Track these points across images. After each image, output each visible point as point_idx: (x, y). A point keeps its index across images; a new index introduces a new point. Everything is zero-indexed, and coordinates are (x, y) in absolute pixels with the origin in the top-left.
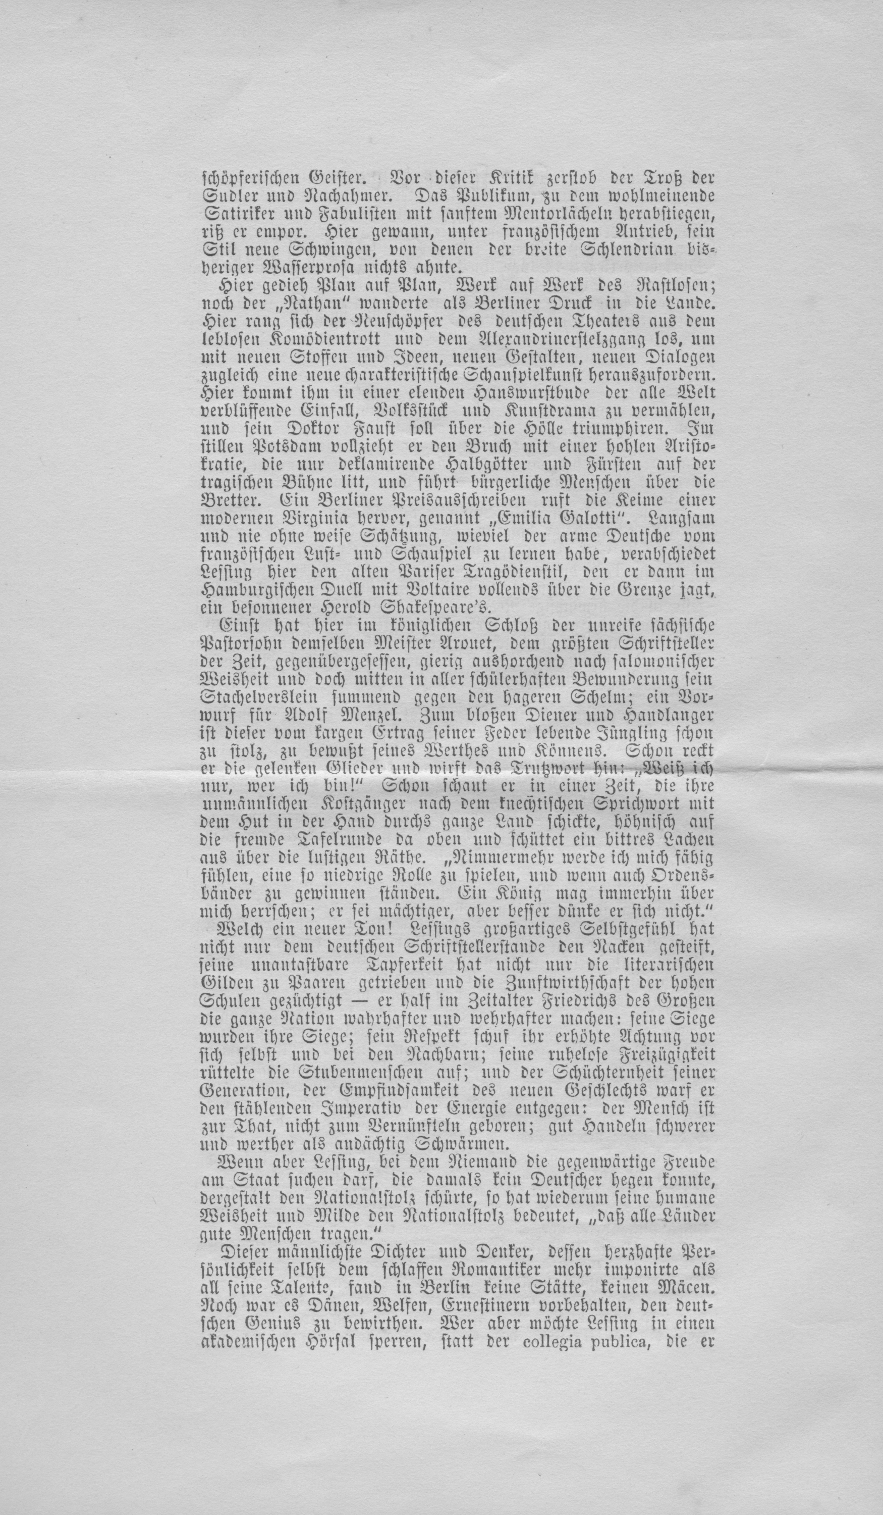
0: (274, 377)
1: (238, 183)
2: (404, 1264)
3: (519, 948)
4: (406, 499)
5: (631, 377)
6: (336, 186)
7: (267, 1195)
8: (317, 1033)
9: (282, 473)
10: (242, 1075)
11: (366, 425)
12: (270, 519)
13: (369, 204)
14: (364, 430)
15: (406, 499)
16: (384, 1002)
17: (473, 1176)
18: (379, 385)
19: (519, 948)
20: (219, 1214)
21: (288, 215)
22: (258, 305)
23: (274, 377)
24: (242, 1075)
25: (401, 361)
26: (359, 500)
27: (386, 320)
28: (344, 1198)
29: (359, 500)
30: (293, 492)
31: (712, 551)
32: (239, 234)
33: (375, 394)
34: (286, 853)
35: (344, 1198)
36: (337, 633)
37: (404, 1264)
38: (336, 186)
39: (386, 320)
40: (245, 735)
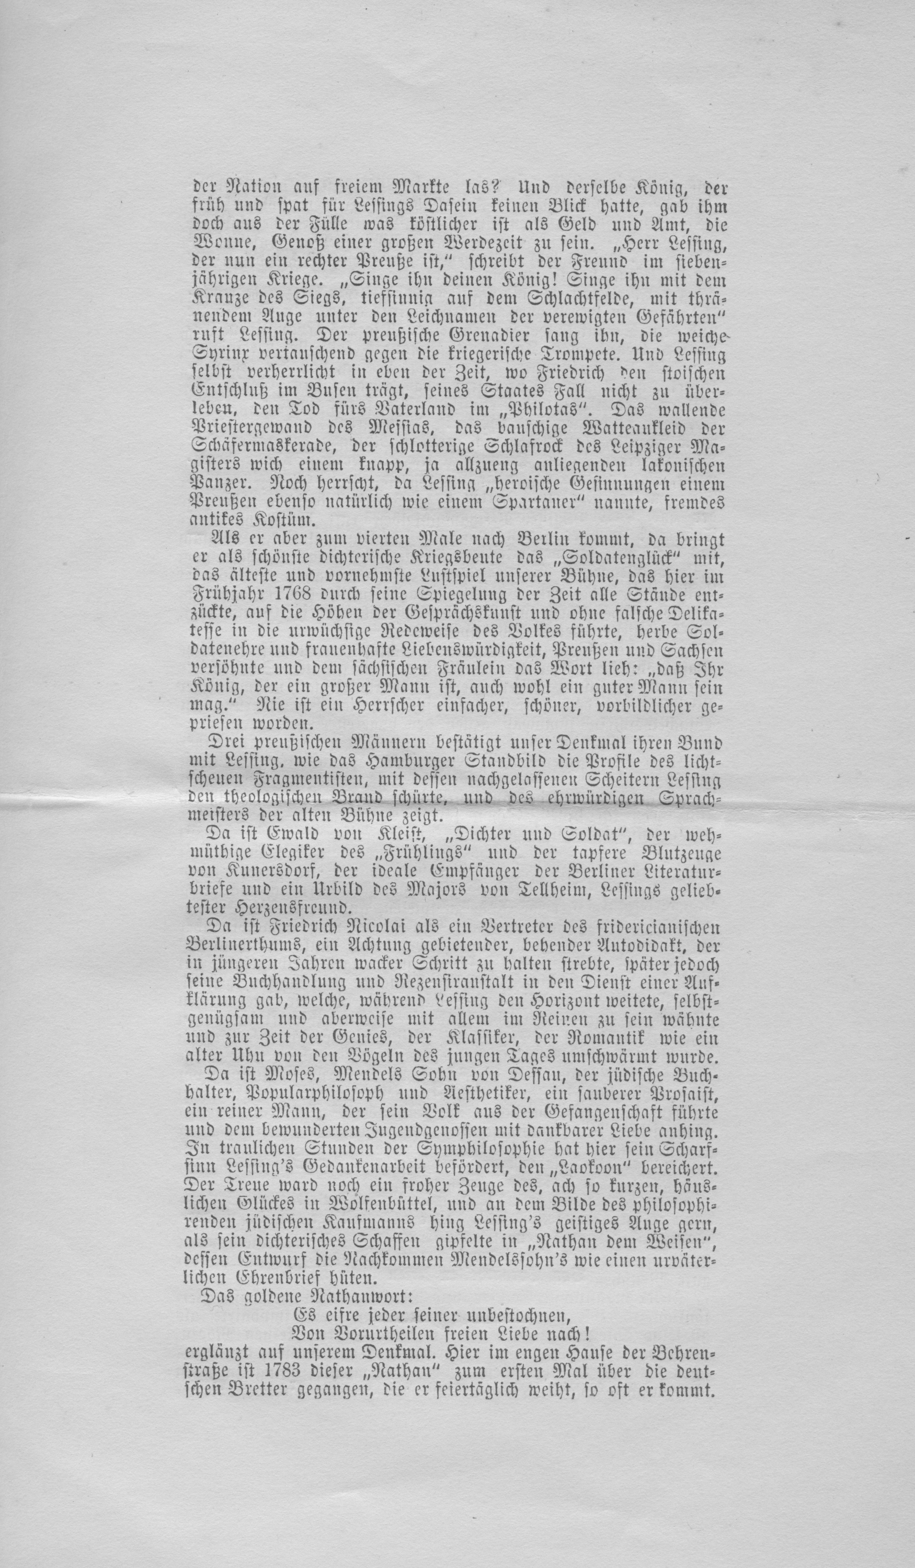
5: (252, 225)
9: (228, 1379)
10: (479, 1243)
11: (566, 388)
12: (253, 502)
13: (229, 658)
14: (565, 393)
16: (256, 540)
18: (315, 456)
20: (463, 241)
24: (479, 1243)
25: (373, 1134)
26: (435, 853)
27: (309, 353)
28: (257, 187)
29: (435, 853)
33: (495, 670)
34: (500, 645)
35: (257, 187)
36: (350, 878)
39: (309, 353)
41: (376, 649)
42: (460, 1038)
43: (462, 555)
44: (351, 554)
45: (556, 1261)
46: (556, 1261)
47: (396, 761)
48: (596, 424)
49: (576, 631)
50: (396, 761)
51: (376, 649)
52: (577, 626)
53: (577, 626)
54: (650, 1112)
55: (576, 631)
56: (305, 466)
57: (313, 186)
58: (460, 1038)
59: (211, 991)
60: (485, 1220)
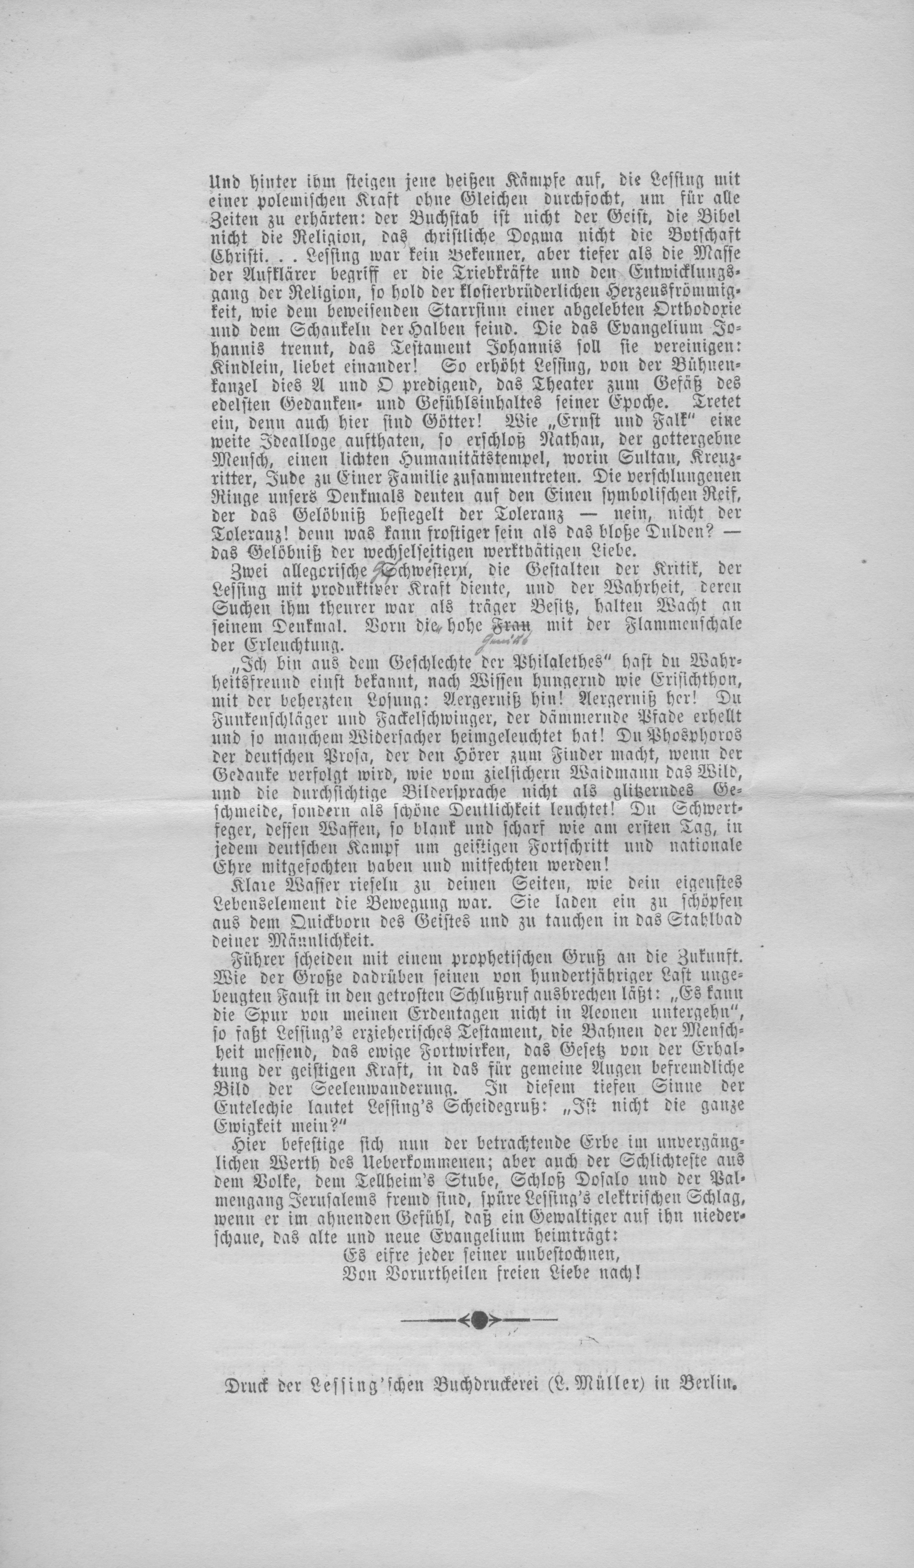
0: (316, 684)
1: (719, 906)
2: (467, 398)
3: (322, 406)
4: (338, 755)
6: (420, 727)
7: (441, 512)
8: (667, 1083)
15: (338, 755)
17: (644, 250)
19: (322, 406)
21: (520, 1256)
22: (475, 516)
23: (316, 684)
30: (683, 374)
31: (350, 1104)
32: (400, 276)
35: (695, 845)
37: (467, 398)
38: (420, 727)
40: (547, 1089)
41: (386, 200)
42: (244, 887)
43: (561, 992)
44: (545, 733)
45: (422, 1108)
46: (422, 1108)
47: (491, 478)
48: (617, 583)
49: (686, 198)
50: (491, 478)
51: (386, 200)
52: (686, 193)
53: (686, 193)
54: (728, 234)
55: (686, 198)
56: (404, 961)
57: (643, 1216)
58: (244, 887)
59: (592, 765)
60: (317, 253)
